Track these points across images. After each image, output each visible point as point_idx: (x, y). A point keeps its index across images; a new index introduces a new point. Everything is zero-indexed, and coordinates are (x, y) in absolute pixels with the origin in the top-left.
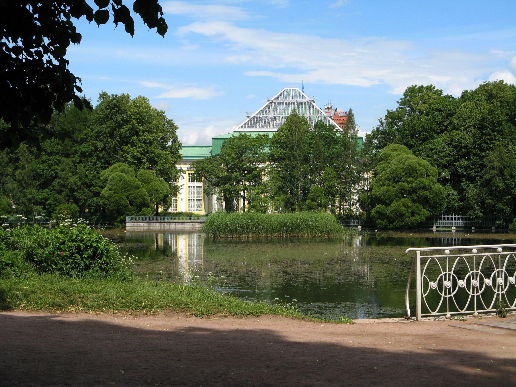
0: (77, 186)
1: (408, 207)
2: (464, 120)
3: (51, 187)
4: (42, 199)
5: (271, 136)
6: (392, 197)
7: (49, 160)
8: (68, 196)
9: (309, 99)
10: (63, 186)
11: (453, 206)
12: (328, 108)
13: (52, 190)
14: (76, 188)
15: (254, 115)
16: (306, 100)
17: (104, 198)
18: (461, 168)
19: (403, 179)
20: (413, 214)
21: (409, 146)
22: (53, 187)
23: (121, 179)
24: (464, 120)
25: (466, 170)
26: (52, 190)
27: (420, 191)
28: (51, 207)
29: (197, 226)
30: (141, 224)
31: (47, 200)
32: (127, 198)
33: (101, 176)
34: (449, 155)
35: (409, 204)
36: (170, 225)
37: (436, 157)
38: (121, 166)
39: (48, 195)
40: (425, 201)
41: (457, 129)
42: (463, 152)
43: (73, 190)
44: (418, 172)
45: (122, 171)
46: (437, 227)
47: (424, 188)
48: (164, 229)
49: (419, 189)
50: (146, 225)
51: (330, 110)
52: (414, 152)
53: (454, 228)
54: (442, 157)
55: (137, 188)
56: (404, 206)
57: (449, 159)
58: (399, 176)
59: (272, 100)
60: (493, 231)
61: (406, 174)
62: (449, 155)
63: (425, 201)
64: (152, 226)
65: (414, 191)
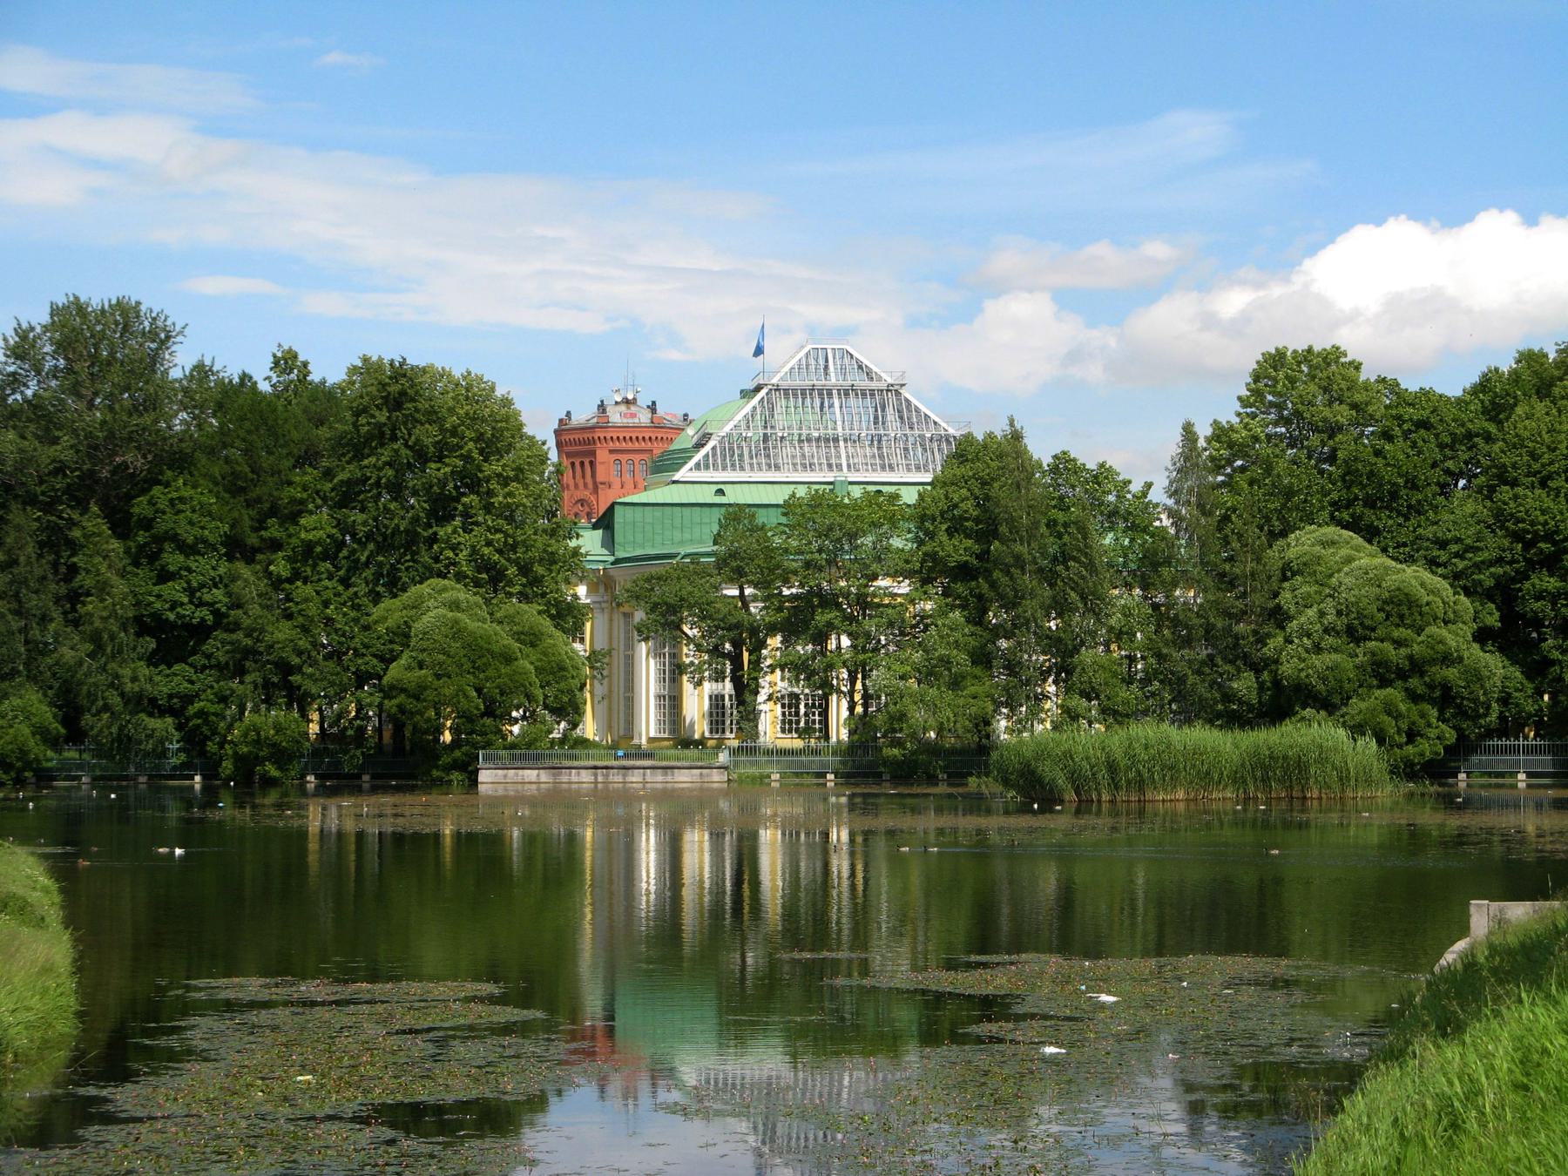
0: (300, 653)
1: (1397, 716)
2: (1534, 456)
3: (197, 659)
4: (171, 696)
5: (909, 496)
6: (1347, 686)
7: (189, 570)
8: (267, 685)
9: (890, 381)
10: (249, 653)
11: (1520, 712)
12: (627, 402)
13: (204, 668)
14: (296, 660)
15: (727, 429)
16: (883, 386)
17: (403, 690)
18: (1538, 598)
19: (1380, 632)
20: (1412, 736)
21: (1370, 534)
22: (209, 656)
23: (457, 631)
24: (1534, 456)
25: (1554, 604)
26: (204, 668)
27: (1433, 669)
28: (206, 722)
29: (716, 778)
30: (531, 775)
31: (188, 699)
32: (479, 690)
33: (376, 622)
34: (1500, 561)
35: (1403, 707)
36: (624, 776)
37: (1461, 565)
38: (445, 589)
39: (192, 682)
40: (1445, 698)
41: (1514, 483)
42: (1541, 550)
43: (286, 669)
44: (1425, 609)
45: (455, 605)
46: (1468, 774)
47: (1447, 659)
48: (607, 789)
49: (1433, 662)
50: (544, 776)
51: (633, 409)
52: (1384, 550)
53: (1522, 776)
54: (1478, 567)
55: (508, 659)
56: (1389, 714)
57: (1500, 571)
58: (1368, 622)
59: (775, 381)
60: (366, 786)
61: (1387, 618)
62: (1500, 561)
63: (1445, 698)
64: (565, 779)
65: (1417, 666)
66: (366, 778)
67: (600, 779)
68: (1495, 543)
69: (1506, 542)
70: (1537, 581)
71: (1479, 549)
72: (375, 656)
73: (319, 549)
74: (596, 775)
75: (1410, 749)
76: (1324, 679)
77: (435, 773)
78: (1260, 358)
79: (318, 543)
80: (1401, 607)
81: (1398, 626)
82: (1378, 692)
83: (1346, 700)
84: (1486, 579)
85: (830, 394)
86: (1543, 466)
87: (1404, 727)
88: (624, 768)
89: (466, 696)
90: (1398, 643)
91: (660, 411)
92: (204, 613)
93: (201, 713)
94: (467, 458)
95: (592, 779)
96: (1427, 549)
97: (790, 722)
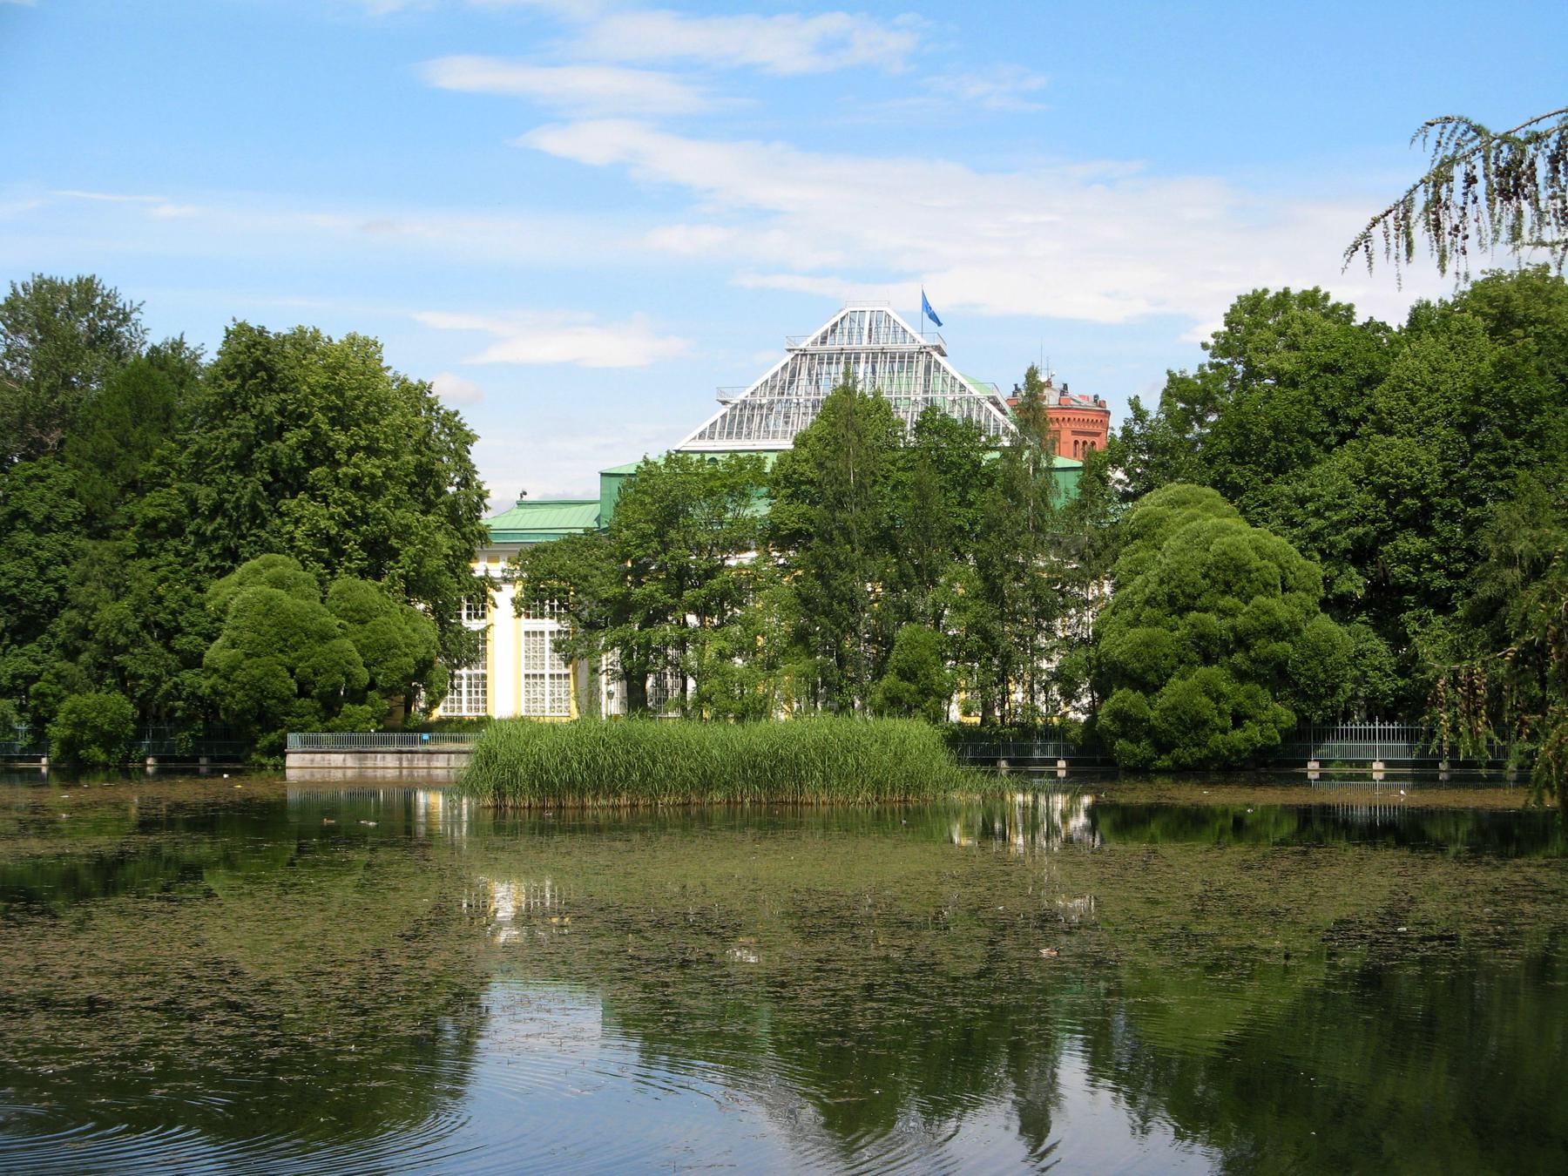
1: (1218, 697)
7: (37, 546)
9: (924, 342)
11: (1373, 692)
17: (216, 671)
19: (1204, 601)
20: (1238, 719)
21: (1231, 491)
24: (1413, 401)
30: (337, 759)
32: (291, 671)
34: (1360, 520)
36: (429, 761)
37: (1316, 524)
40: (1278, 677)
41: (1388, 431)
42: (1406, 507)
46: (1323, 764)
47: (1275, 631)
49: (1257, 634)
50: (350, 761)
52: (1243, 511)
53: (1378, 766)
54: (1337, 527)
55: (324, 637)
56: (1207, 693)
57: (1360, 530)
58: (1188, 590)
59: (803, 346)
61: (1213, 586)
62: (1360, 520)
63: (1278, 677)
64: (370, 763)
65: (1242, 641)
66: (203, 761)
67: (405, 764)
68: (1361, 499)
69: (1370, 499)
70: (1400, 543)
71: (1342, 507)
72: (199, 634)
73: (163, 525)
74: (401, 760)
75: (1237, 735)
76: (1137, 656)
77: (254, 757)
78: (1235, 301)
79: (163, 519)
80: (1231, 576)
81: (1224, 593)
82: (1202, 669)
83: (1164, 678)
84: (1343, 541)
85: (857, 359)
86: (1421, 410)
87: (1227, 708)
88: (429, 752)
89: (276, 676)
90: (1224, 613)
91: (1071, 391)
92: (49, 591)
93: (40, 695)
94: (315, 428)
95: (397, 764)
96: (1287, 508)
97: (477, 701)
